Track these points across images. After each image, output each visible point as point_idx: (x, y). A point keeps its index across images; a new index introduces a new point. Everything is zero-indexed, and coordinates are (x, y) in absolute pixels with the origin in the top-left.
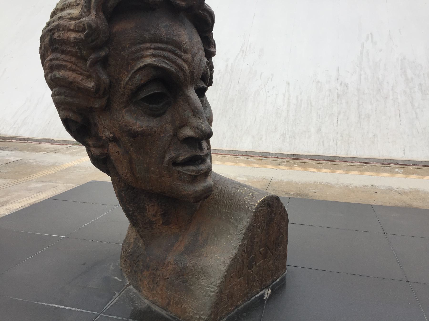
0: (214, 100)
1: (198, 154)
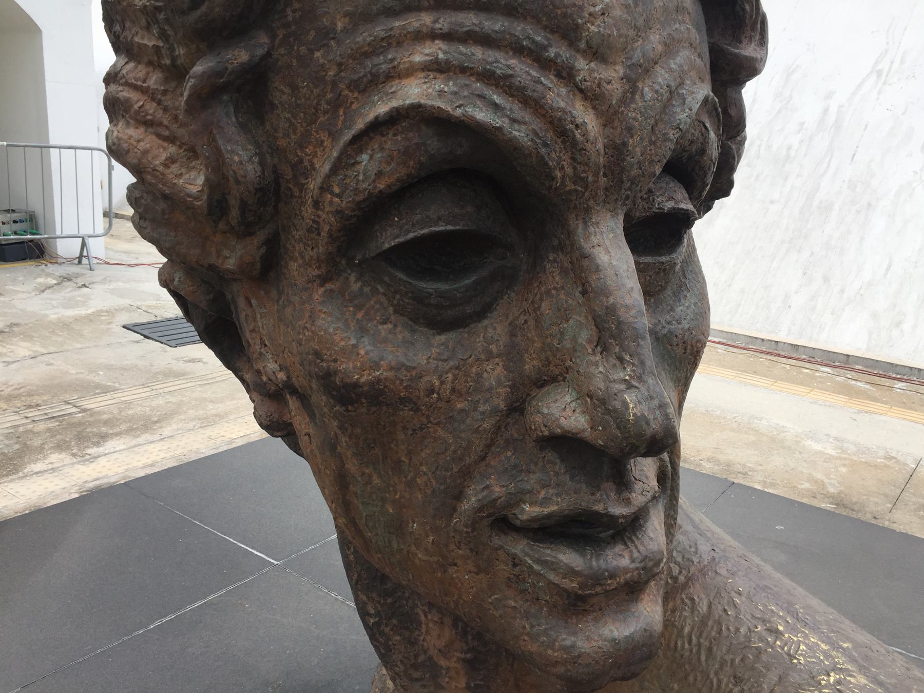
0: (772, 202)
1: (599, 508)
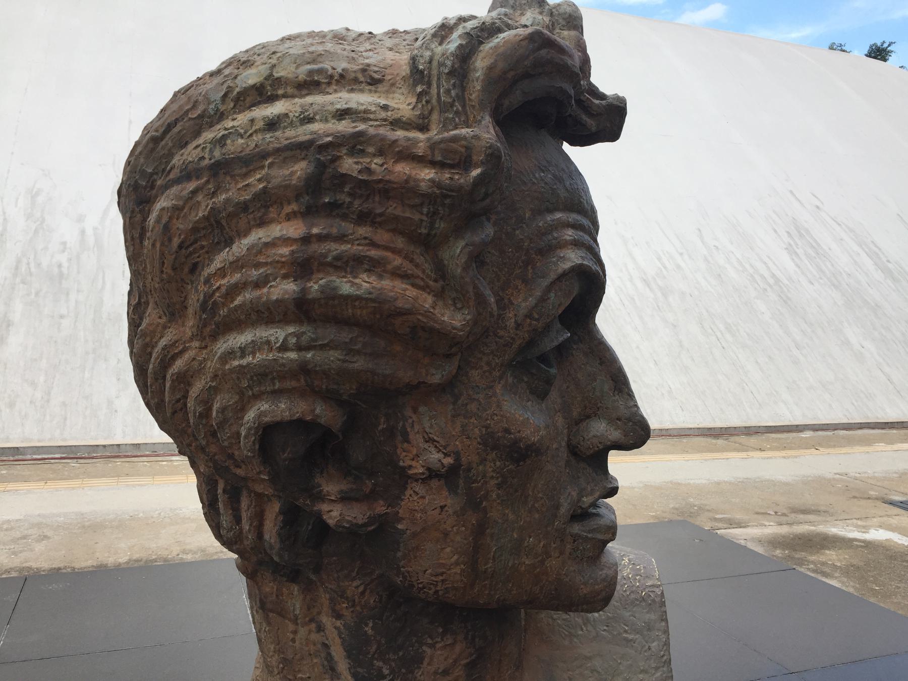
0: (62, 317)
